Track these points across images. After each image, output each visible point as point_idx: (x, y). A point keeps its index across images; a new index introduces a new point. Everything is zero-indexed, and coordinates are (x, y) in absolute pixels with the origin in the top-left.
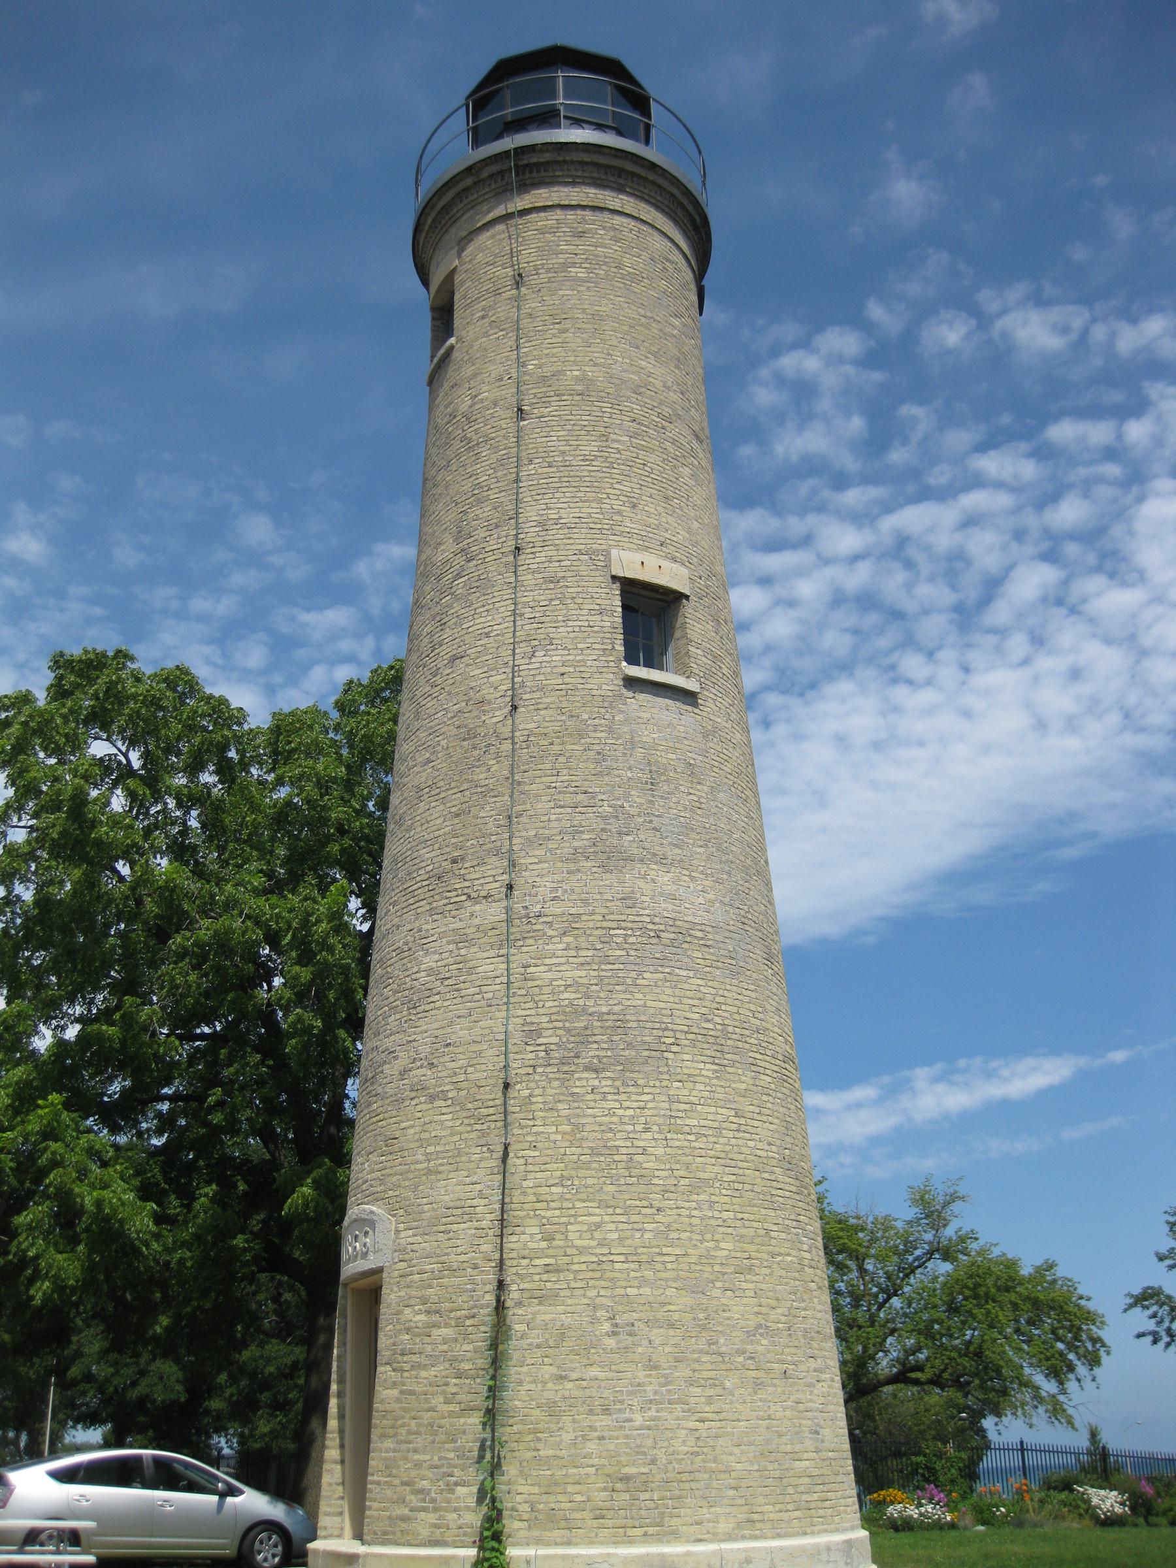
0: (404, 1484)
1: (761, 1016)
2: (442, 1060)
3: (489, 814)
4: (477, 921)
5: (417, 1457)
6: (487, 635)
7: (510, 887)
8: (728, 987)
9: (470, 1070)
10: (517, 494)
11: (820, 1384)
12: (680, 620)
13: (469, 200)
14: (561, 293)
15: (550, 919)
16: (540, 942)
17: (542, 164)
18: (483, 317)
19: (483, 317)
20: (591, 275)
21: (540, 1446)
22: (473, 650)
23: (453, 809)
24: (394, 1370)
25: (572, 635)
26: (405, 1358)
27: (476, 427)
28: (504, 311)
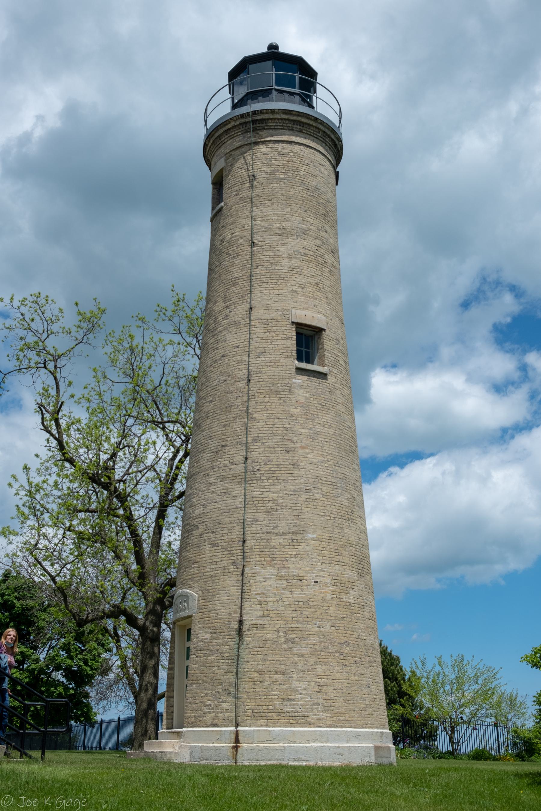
0: (201, 702)
1: (350, 514)
2: (217, 530)
3: (238, 426)
4: (232, 472)
5: (206, 692)
6: (238, 347)
7: (246, 459)
8: (337, 502)
9: (229, 534)
10: (251, 282)
11: (371, 668)
12: (322, 340)
13: (230, 134)
14: (272, 185)
15: (263, 472)
16: (259, 482)
17: (265, 119)
18: (236, 195)
19: (236, 195)
20: (286, 176)
21: (256, 687)
22: (232, 353)
23: (223, 424)
24: (197, 657)
25: (274, 349)
26: (202, 652)
27: (233, 248)
28: (246, 193)
